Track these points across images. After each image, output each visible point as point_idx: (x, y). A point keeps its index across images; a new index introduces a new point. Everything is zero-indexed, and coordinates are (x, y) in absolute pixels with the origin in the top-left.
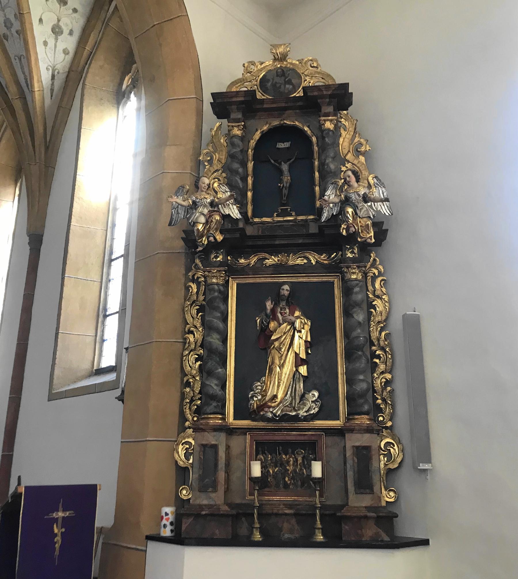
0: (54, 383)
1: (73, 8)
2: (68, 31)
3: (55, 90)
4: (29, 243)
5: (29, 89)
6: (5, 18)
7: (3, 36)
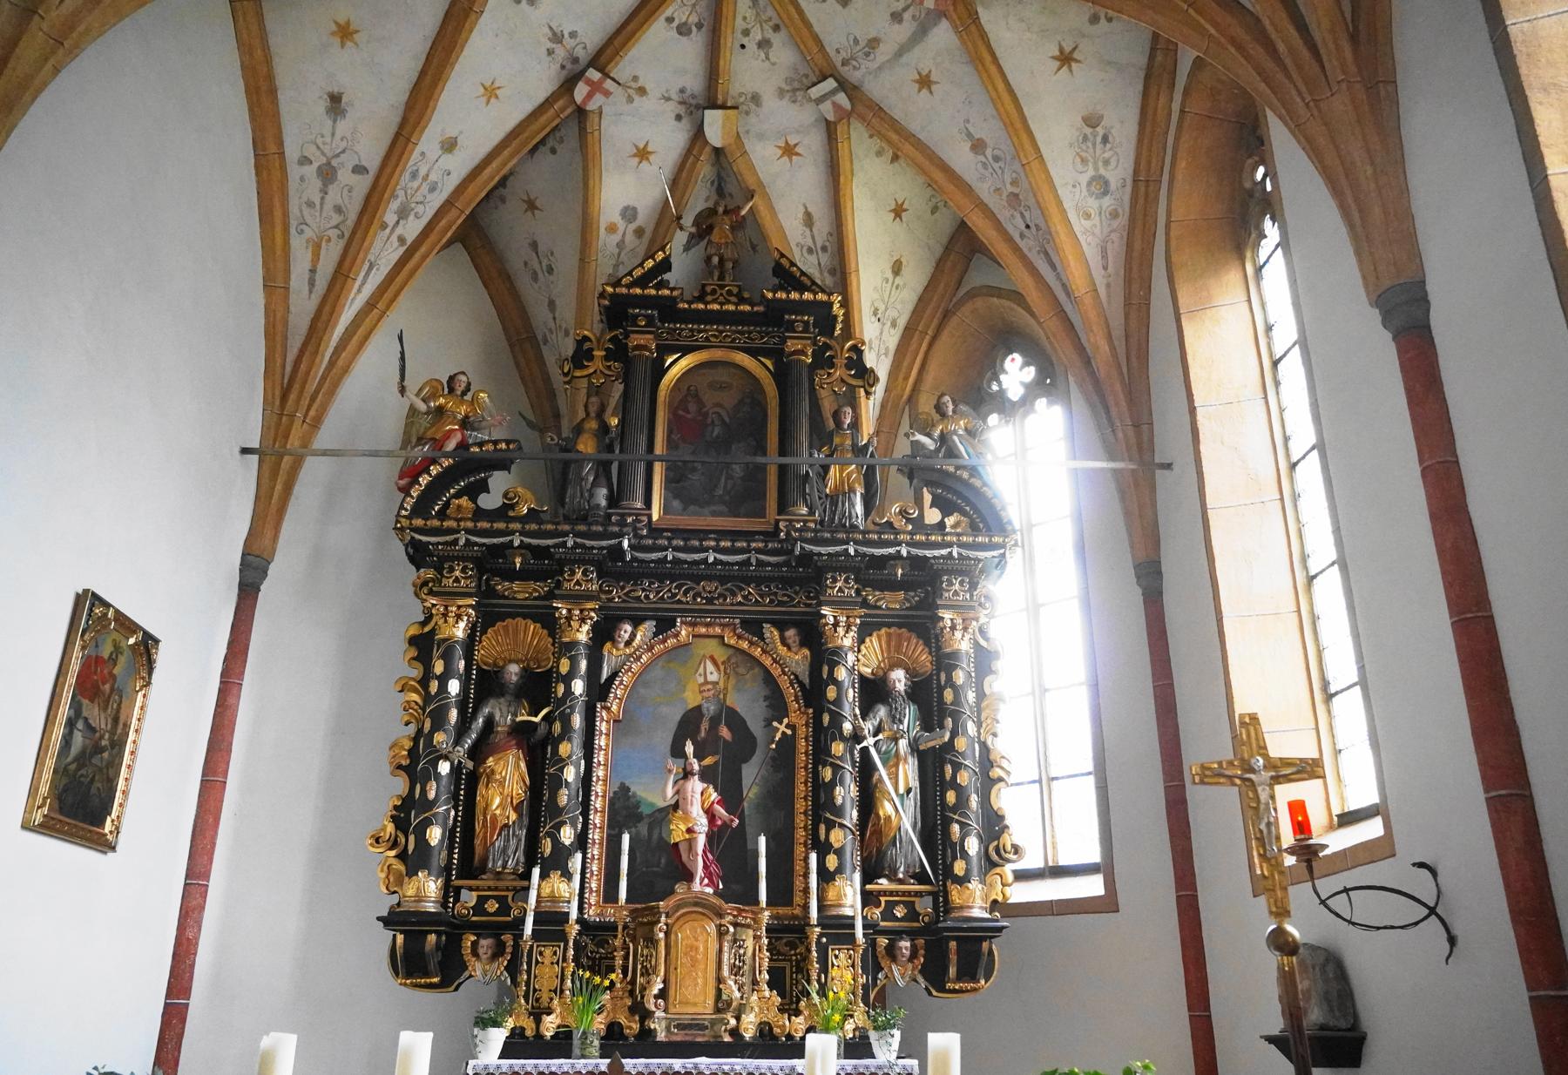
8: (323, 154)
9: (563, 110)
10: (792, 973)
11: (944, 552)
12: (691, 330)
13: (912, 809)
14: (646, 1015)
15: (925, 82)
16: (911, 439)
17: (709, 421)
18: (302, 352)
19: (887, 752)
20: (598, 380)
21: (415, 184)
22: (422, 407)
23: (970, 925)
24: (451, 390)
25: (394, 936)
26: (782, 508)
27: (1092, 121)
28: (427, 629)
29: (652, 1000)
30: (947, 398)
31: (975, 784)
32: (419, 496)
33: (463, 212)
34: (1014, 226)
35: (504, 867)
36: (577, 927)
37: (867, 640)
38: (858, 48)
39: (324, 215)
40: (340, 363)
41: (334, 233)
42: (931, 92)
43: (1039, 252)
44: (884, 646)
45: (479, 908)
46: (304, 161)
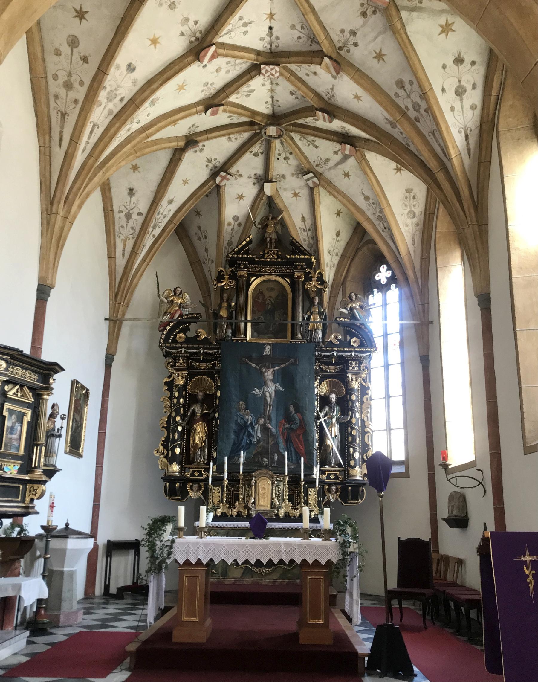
0: (526, 437)
1: (471, 62)
2: (471, 87)
4: (478, 304)
5: (447, 158)
7: (415, 120)
8: (127, 209)
9: (212, 186)
10: (296, 496)
11: (349, 354)
12: (260, 267)
13: (337, 442)
14: (249, 509)
15: (347, 175)
16: (339, 311)
17: (267, 302)
18: (121, 280)
19: (328, 423)
20: (226, 287)
21: (159, 217)
22: (166, 301)
23: (355, 482)
24: (175, 294)
25: (166, 484)
26: (293, 336)
27: (409, 191)
28: (170, 380)
29: (251, 505)
30: (353, 294)
31: (359, 434)
32: (166, 334)
33: (176, 225)
34: (380, 227)
35: (200, 461)
36: (227, 481)
37: (322, 383)
38: (322, 161)
39: (127, 230)
40: (134, 283)
41: (131, 237)
42: (349, 179)
43: (389, 238)
44: (328, 384)
45: (192, 475)
46: (120, 212)
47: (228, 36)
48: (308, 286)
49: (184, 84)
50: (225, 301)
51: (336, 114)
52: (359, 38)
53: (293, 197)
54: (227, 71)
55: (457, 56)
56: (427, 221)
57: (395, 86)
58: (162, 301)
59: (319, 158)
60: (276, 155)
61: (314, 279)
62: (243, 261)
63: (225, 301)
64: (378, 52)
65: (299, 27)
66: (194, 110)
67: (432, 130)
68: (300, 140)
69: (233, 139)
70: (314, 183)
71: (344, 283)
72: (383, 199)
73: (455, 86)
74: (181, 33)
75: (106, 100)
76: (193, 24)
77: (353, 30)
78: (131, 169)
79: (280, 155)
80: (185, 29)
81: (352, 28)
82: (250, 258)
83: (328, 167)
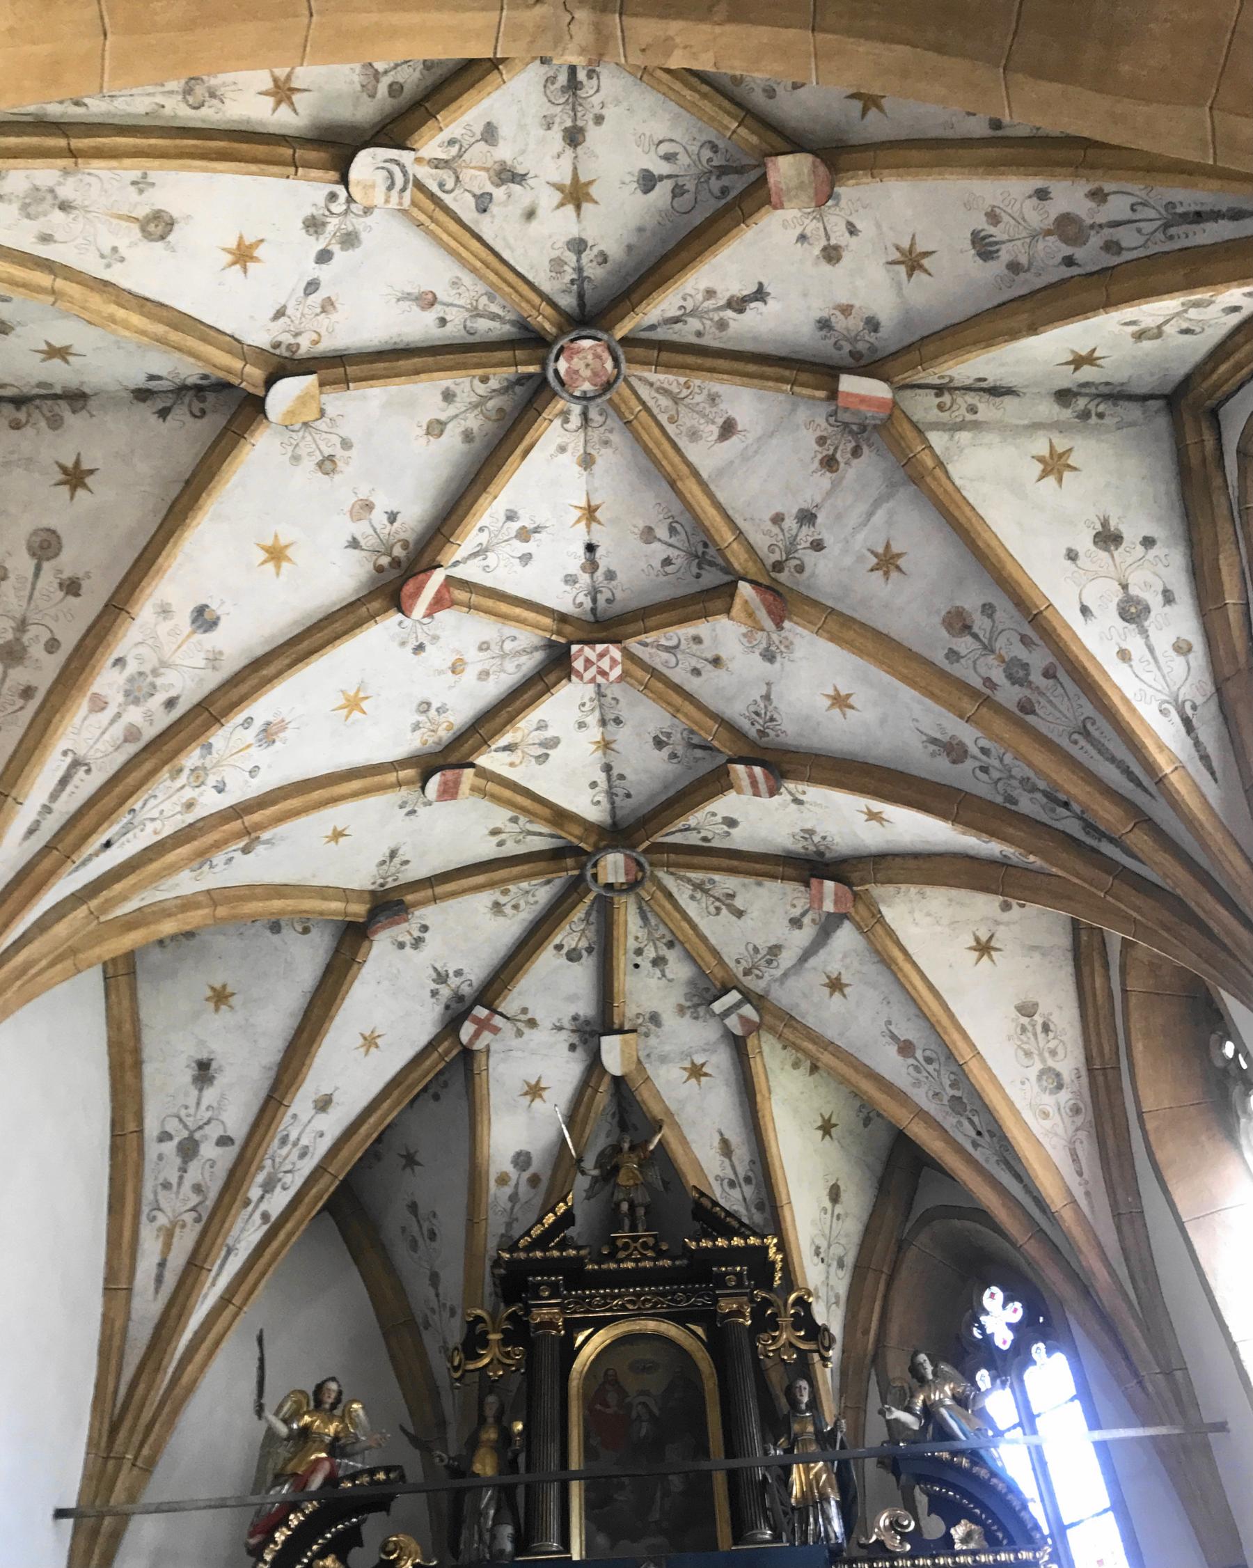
2: (1160, 598)
3: (1213, 757)
6: (1004, 665)
8: (186, 1126)
9: (447, 1052)
12: (604, 1297)
15: (836, 985)
17: (634, 1414)
20: (495, 1373)
21: (284, 1151)
22: (283, 1430)
24: (319, 1403)
27: (1027, 1010)
32: (274, 1560)
34: (964, 1133)
38: (759, 956)
39: (181, 1197)
41: (189, 1218)
42: (844, 996)
46: (165, 1137)
47: (477, 561)
48: (767, 1345)
49: (361, 695)
50: (490, 1420)
51: (786, 767)
52: (823, 528)
53: (688, 1079)
54: (480, 674)
55: (1099, 528)
56: (1102, 1092)
57: (944, 633)
58: (271, 1434)
59: (750, 947)
60: (631, 954)
61: (785, 1321)
62: (549, 1276)
63: (490, 1420)
64: (880, 550)
65: (662, 532)
66: (391, 777)
67: (1081, 724)
68: (692, 898)
69: (508, 910)
70: (744, 1020)
71: (878, 1357)
72: (956, 1036)
73: (1116, 600)
74: (350, 539)
75: (120, 698)
76: (386, 522)
77: (807, 511)
78: (208, 999)
79: (639, 952)
80: (361, 530)
81: (805, 506)
82: (569, 1258)
83: (778, 973)
